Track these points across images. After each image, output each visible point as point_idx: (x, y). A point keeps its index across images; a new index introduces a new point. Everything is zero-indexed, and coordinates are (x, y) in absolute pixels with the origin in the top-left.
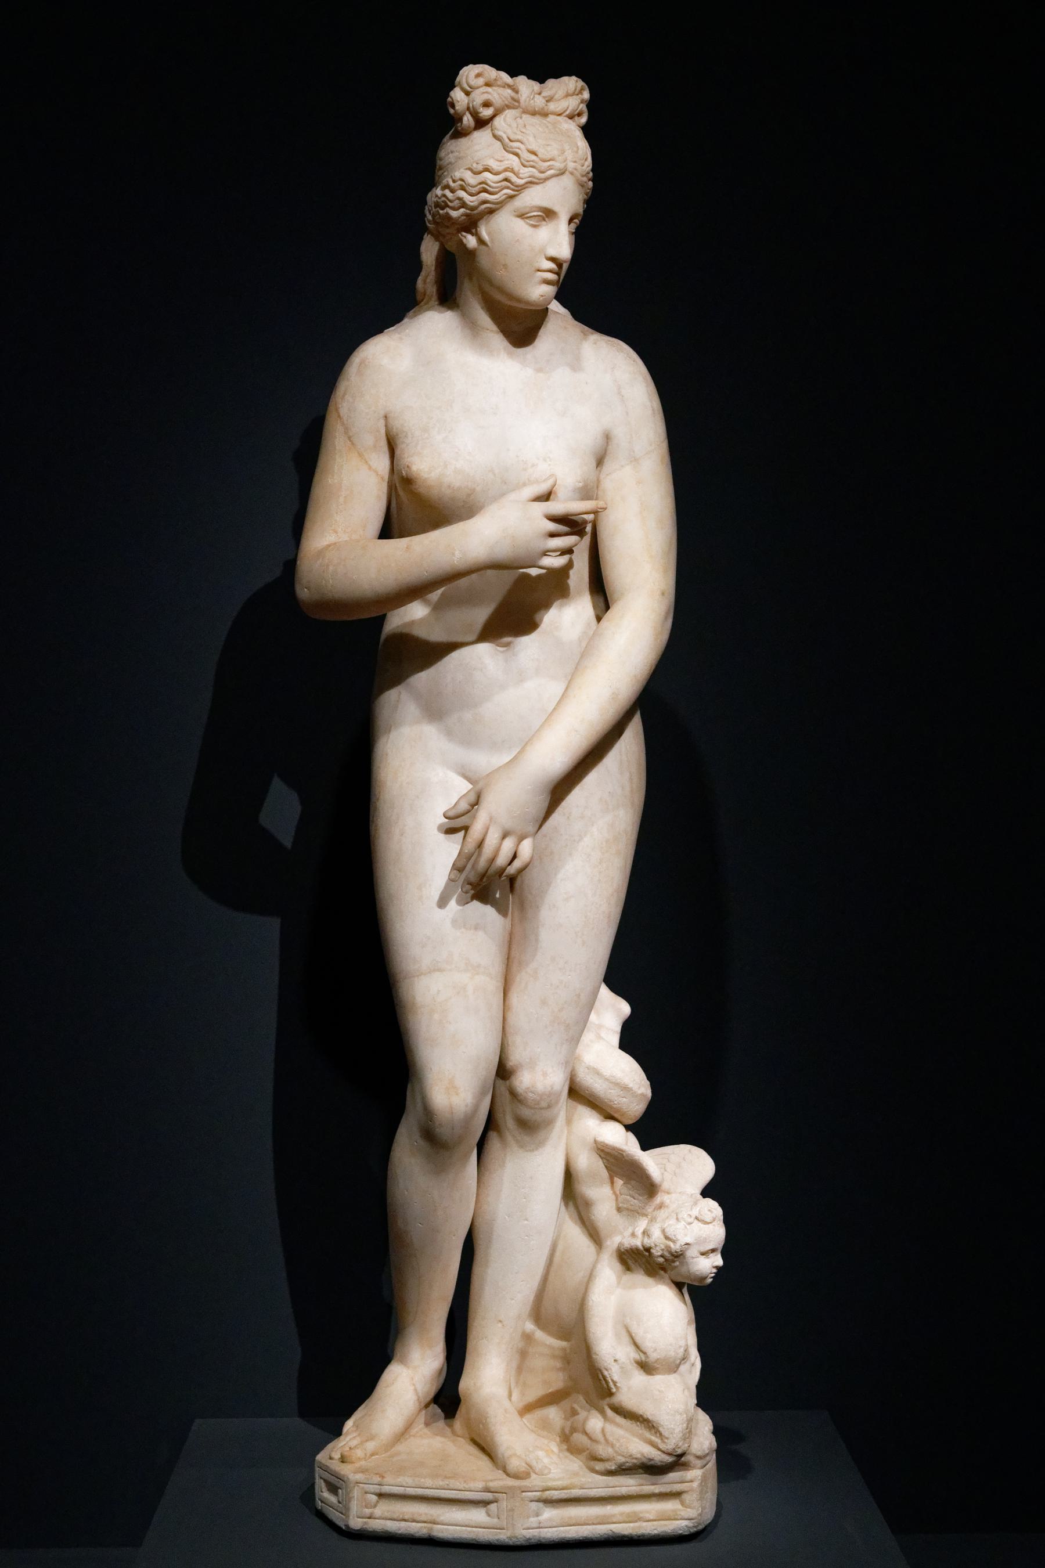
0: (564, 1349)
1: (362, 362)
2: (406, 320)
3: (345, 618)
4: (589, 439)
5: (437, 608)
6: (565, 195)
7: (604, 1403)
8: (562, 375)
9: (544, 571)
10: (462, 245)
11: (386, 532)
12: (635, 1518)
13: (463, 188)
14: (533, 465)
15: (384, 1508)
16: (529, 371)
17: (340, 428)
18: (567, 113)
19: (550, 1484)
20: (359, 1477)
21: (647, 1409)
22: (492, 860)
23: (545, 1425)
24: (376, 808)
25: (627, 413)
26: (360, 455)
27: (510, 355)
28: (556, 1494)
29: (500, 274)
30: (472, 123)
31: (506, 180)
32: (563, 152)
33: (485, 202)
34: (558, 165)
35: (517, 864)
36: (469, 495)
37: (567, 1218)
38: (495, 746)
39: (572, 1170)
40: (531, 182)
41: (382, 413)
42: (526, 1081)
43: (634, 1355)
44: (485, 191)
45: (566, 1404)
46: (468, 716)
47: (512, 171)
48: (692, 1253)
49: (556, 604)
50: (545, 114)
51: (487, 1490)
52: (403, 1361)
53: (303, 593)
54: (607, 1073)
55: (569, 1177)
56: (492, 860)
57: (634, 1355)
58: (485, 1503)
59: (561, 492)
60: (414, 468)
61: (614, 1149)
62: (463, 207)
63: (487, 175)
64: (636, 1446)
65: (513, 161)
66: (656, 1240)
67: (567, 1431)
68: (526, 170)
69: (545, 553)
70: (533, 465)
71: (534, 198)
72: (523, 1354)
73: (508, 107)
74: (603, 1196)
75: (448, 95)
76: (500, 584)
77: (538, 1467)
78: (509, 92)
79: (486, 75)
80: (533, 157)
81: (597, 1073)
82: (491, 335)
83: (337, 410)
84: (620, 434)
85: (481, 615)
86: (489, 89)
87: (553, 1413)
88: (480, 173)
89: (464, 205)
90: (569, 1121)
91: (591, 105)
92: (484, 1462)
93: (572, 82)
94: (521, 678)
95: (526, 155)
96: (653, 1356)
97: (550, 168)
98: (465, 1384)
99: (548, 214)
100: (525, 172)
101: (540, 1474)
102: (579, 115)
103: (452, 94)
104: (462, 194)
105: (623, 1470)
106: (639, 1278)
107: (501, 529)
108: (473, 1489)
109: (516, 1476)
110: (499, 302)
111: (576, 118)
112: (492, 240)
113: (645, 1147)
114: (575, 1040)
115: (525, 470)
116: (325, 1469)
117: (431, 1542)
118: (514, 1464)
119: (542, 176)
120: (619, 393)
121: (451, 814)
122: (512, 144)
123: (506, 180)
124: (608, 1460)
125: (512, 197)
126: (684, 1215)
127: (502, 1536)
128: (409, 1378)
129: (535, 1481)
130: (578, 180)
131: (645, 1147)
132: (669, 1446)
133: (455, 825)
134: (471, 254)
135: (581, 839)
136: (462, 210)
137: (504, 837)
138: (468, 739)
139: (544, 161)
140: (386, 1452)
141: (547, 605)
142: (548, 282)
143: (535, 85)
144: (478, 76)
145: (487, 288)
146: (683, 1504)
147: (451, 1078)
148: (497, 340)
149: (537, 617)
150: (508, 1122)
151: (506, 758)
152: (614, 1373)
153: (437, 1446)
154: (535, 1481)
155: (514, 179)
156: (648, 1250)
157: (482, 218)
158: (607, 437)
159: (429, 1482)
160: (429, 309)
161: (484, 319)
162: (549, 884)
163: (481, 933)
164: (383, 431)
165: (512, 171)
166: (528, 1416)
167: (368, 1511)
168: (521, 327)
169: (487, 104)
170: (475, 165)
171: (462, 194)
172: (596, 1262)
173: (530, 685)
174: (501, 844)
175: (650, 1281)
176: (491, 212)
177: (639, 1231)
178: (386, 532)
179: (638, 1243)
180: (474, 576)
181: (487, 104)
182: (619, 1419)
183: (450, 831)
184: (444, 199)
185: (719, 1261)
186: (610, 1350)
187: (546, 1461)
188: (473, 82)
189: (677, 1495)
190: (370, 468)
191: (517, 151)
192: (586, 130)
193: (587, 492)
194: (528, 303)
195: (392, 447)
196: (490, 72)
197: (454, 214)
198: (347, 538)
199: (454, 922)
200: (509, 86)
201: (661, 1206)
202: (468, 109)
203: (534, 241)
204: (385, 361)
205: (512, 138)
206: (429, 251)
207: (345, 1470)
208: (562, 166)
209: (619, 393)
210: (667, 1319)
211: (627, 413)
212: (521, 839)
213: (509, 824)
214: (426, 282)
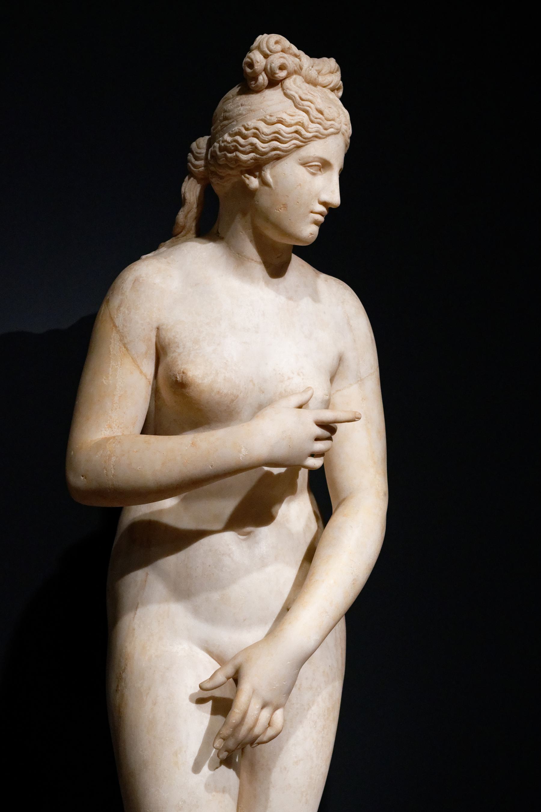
1: (136, 280)
2: (162, 249)
4: (328, 360)
5: (183, 500)
6: (333, 148)
8: (306, 303)
9: (282, 470)
10: (245, 187)
11: (148, 428)
13: (255, 136)
14: (289, 378)
16: (282, 299)
17: (115, 336)
18: (331, 86)
22: (251, 729)
24: (120, 678)
25: (355, 341)
26: (134, 361)
27: (267, 284)
29: (278, 213)
30: (266, 82)
31: (296, 132)
32: (339, 114)
34: (337, 125)
35: (270, 732)
36: (233, 401)
38: (238, 623)
40: (316, 137)
41: (155, 325)
44: (277, 139)
46: (215, 596)
47: (303, 125)
53: (77, 480)
56: (251, 729)
60: (190, 374)
62: (252, 152)
63: (279, 126)
65: (303, 117)
70: (289, 378)
76: (244, 483)
78: (298, 60)
80: (320, 116)
82: (254, 264)
83: (112, 319)
84: (350, 356)
85: (228, 507)
86: (285, 55)
89: (255, 149)
93: (331, 63)
94: (263, 564)
95: (314, 113)
97: (331, 126)
99: (325, 165)
102: (338, 89)
103: (251, 55)
104: (255, 140)
107: (268, 434)
111: (336, 91)
112: (276, 182)
121: (208, 685)
122: (303, 102)
125: (298, 147)
134: (251, 193)
135: (309, 708)
136: (252, 155)
137: (263, 707)
138: (213, 617)
139: (328, 120)
141: (279, 500)
142: (316, 223)
144: (277, 42)
145: (260, 223)
149: (274, 510)
155: (303, 132)
157: (268, 163)
160: (186, 240)
161: (250, 250)
163: (227, 796)
164: (154, 340)
169: (282, 68)
170: (268, 117)
173: (270, 569)
174: (259, 714)
176: (278, 158)
178: (148, 428)
183: (200, 701)
184: (235, 144)
190: (141, 372)
191: (308, 108)
194: (298, 239)
195: (161, 352)
196: (286, 43)
197: (244, 157)
198: (119, 434)
199: (207, 786)
200: (296, 56)
202: (265, 70)
203: (309, 189)
204: (158, 280)
205: (304, 97)
206: (191, 190)
211: (355, 341)
212: (276, 709)
214: (187, 216)
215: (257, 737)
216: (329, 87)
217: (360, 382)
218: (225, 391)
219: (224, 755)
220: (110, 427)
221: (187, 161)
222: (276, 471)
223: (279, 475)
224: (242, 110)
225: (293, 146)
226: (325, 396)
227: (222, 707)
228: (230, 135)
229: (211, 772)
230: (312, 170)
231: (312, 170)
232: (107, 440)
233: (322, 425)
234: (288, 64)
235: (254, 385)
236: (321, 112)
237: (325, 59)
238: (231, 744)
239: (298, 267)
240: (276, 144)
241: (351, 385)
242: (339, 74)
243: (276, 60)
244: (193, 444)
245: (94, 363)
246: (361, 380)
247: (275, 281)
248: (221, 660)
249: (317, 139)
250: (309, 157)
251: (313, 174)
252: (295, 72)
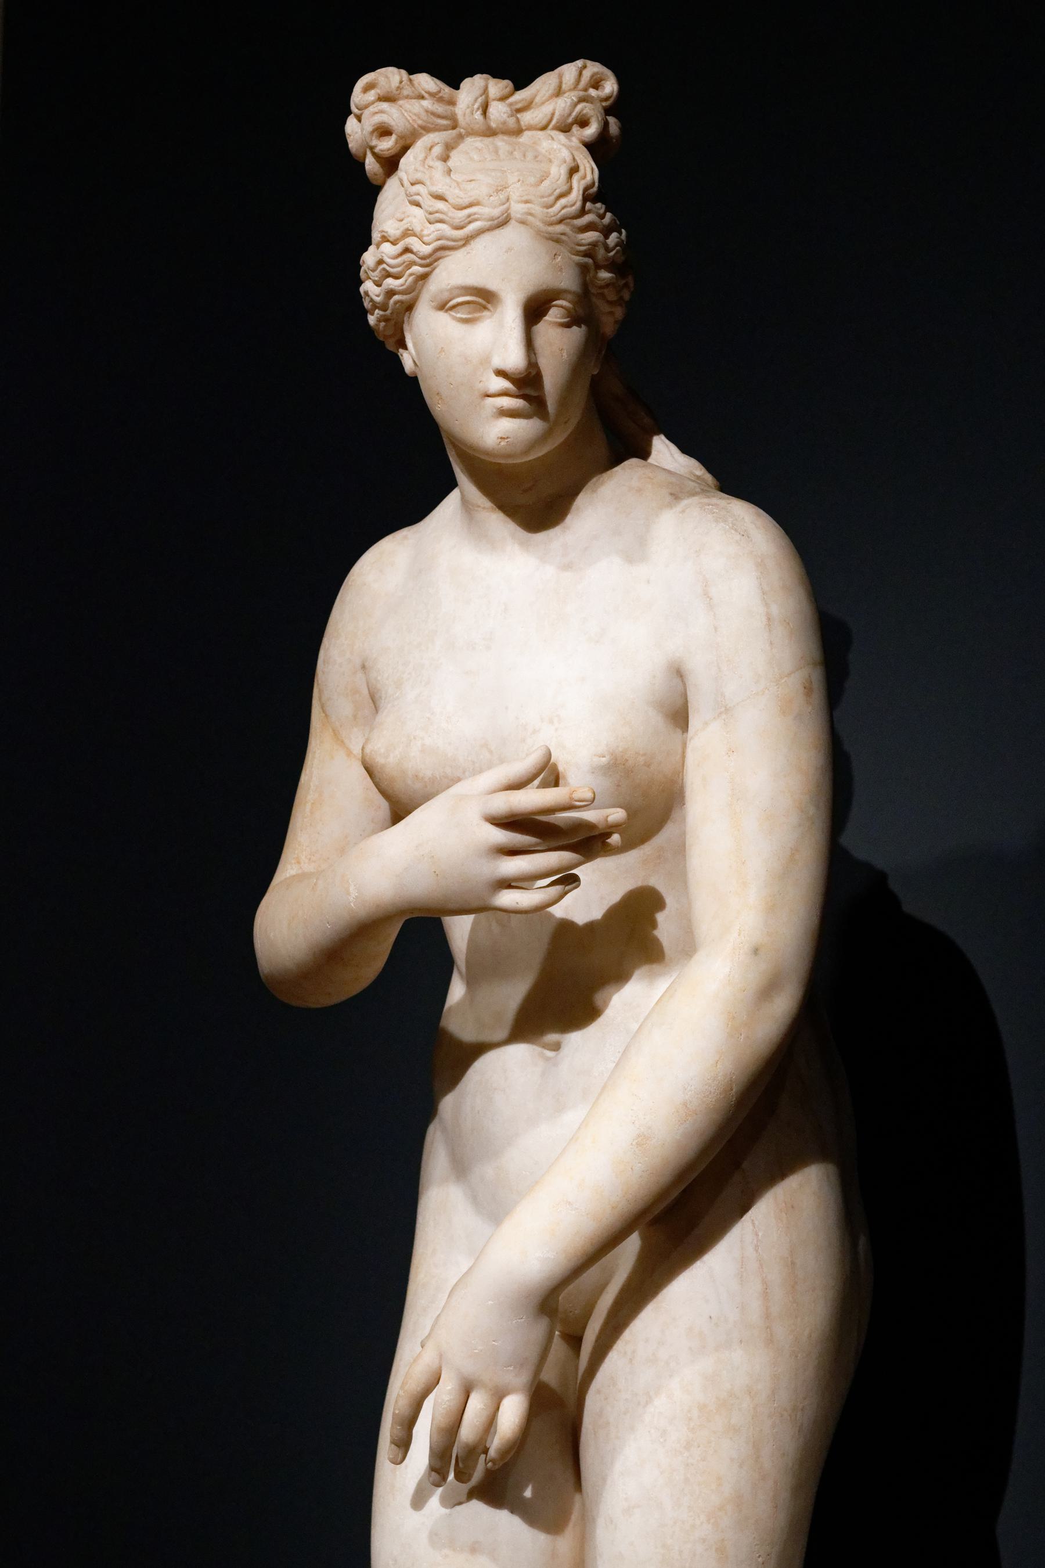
26: (336, 734)
27: (523, 544)
31: (407, 250)
40: (443, 248)
49: (638, 974)
68: (432, 227)
71: (453, 273)
73: (427, 129)
79: (382, 81)
80: (440, 205)
86: (385, 105)
99: (484, 299)
100: (431, 231)
102: (583, 123)
110: (514, 464)
115: (523, 740)
120: (706, 595)
125: (424, 277)
130: (539, 233)
135: (649, 1401)
141: (620, 977)
148: (498, 523)
149: (599, 998)
158: (678, 673)
162: (604, 1479)
168: (536, 499)
199: (434, 1538)
208: (496, 212)
209: (706, 595)
213: (470, 1368)
216: (551, 126)
217: (724, 716)
218: (429, 773)
225: (411, 279)
226: (596, 759)
229: (448, 1511)
230: (459, 315)
231: (459, 315)
234: (393, 123)
235: (491, 752)
236: (440, 198)
241: (706, 724)
246: (727, 710)
249: (447, 253)
250: (441, 291)
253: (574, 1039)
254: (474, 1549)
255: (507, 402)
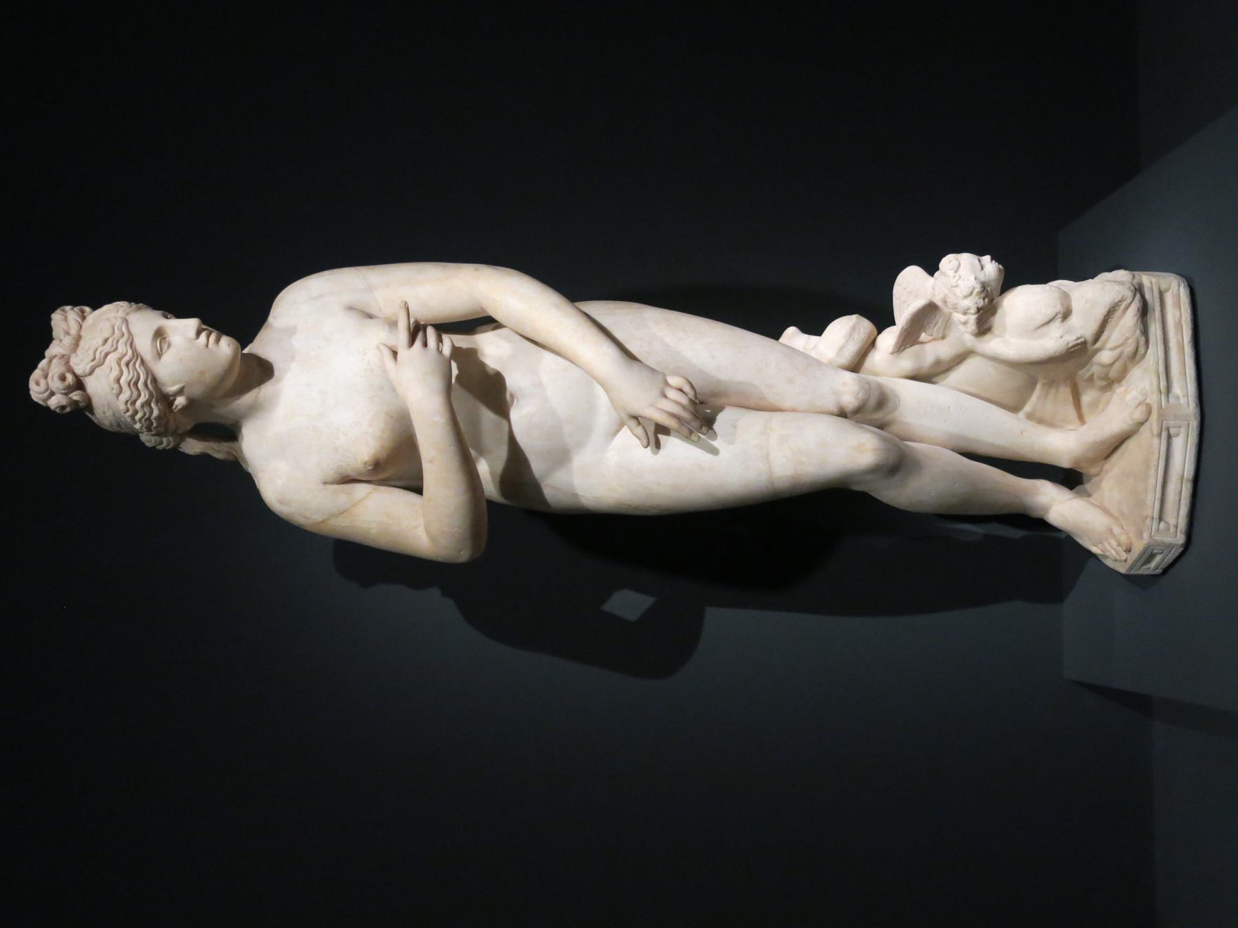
0: (1044, 384)
1: (281, 502)
2: (250, 470)
3: (486, 520)
4: (350, 322)
5: (481, 452)
6: (143, 322)
7: (1091, 348)
8: (298, 342)
10: (185, 409)
11: (419, 490)
12: (1179, 325)
13: (134, 403)
15: (1170, 518)
19: (1155, 387)
20: (1146, 536)
21: (1100, 312)
23: (1094, 405)
24: (637, 508)
26: (354, 506)
28: (1163, 383)
29: (209, 378)
31: (127, 365)
32: (108, 319)
33: (146, 384)
34: (118, 323)
35: (687, 388)
36: (391, 417)
37: (945, 382)
39: (912, 374)
40: (131, 345)
42: (849, 400)
43: (1058, 321)
44: (136, 384)
45: (1081, 385)
47: (121, 359)
48: (982, 278)
50: (79, 338)
51: (1160, 435)
52: (1046, 509)
53: (464, 556)
54: (842, 341)
55: (915, 377)
57: (1058, 321)
58: (1169, 437)
59: (392, 342)
61: (900, 336)
63: (122, 381)
64: (1128, 320)
65: (112, 358)
66: (973, 303)
67: (1104, 383)
69: (440, 352)
71: (144, 344)
72: (1041, 421)
74: (933, 349)
75: (54, 412)
76: (463, 399)
77: (1140, 398)
78: (54, 361)
80: (110, 341)
81: (842, 348)
82: (261, 394)
83: (318, 523)
84: (348, 298)
85: (488, 416)
87: (1087, 398)
88: (121, 388)
89: (147, 403)
90: (876, 374)
91: (75, 303)
92: (1131, 445)
93: (57, 318)
94: (539, 385)
95: (107, 347)
96: (1059, 308)
97: (120, 329)
98: (1065, 464)
99: (159, 334)
100: (122, 348)
101: (1146, 395)
102: (83, 312)
103: (52, 408)
104: (138, 404)
105: (1145, 332)
106: (997, 320)
107: (419, 388)
108: (1159, 445)
109: (1149, 412)
112: (179, 382)
113: (894, 323)
114: (818, 363)
116: (1132, 567)
117: (1196, 480)
118: (1139, 415)
119: (126, 335)
121: (645, 442)
123: (127, 365)
124: (1138, 343)
125: (143, 362)
126: (953, 282)
127: (1194, 424)
128: (1058, 506)
129: (1153, 399)
131: (894, 323)
132: (1129, 294)
133: (656, 434)
134: (192, 403)
136: (153, 405)
137: (665, 396)
139: (113, 333)
140: (1121, 518)
142: (218, 340)
143: (54, 342)
144: (38, 384)
146: (1167, 290)
147: (846, 452)
148: (266, 390)
149: (491, 373)
150: (878, 416)
151: (600, 391)
152: (1071, 339)
153: (1111, 484)
154: (1153, 399)
156: (979, 310)
159: (1152, 481)
161: (247, 399)
164: (335, 486)
165: (121, 359)
166: (1087, 418)
167: (1172, 529)
168: (259, 371)
169: (63, 378)
171: (138, 404)
172: (984, 356)
175: (1000, 312)
176: (155, 380)
177: (962, 318)
178: (419, 490)
179: (972, 318)
180: (459, 418)
181: (63, 378)
182: (1103, 337)
183: (658, 445)
185: (987, 258)
186: (1053, 341)
187: (1134, 393)
188: (42, 387)
189: (1161, 294)
192: (95, 307)
193: (393, 324)
195: (347, 480)
196: (37, 374)
197: (156, 413)
199: (731, 441)
200: (50, 361)
201: (945, 302)
202: (66, 394)
203: (184, 349)
204: (279, 482)
205: (91, 357)
206: (193, 447)
207: (1138, 547)
210: (1028, 302)
212: (667, 384)
214: (217, 450)
215: (691, 400)
219: (704, 429)
220: (416, 527)
221: (164, 450)
222: (455, 372)
223: (459, 368)
224: (109, 413)
227: (662, 429)
228: (135, 422)
232: (427, 532)
233: (412, 341)
236: (106, 341)
237: (53, 323)
238: (696, 424)
239: (262, 346)
240: (140, 385)
242: (68, 308)
243: (56, 384)
244: (430, 462)
245: (358, 538)
247: (276, 373)
248: (621, 425)
251: (169, 346)
252: (67, 362)
253: (510, 383)
254: (735, 427)
255: (213, 337)
